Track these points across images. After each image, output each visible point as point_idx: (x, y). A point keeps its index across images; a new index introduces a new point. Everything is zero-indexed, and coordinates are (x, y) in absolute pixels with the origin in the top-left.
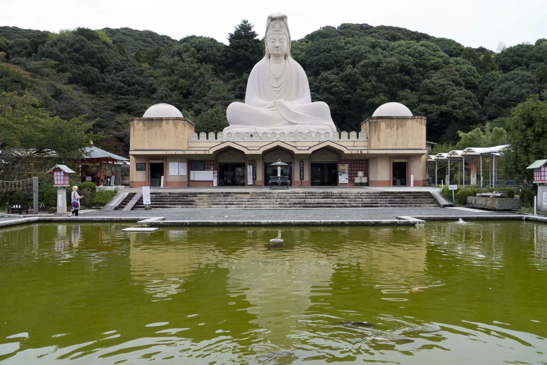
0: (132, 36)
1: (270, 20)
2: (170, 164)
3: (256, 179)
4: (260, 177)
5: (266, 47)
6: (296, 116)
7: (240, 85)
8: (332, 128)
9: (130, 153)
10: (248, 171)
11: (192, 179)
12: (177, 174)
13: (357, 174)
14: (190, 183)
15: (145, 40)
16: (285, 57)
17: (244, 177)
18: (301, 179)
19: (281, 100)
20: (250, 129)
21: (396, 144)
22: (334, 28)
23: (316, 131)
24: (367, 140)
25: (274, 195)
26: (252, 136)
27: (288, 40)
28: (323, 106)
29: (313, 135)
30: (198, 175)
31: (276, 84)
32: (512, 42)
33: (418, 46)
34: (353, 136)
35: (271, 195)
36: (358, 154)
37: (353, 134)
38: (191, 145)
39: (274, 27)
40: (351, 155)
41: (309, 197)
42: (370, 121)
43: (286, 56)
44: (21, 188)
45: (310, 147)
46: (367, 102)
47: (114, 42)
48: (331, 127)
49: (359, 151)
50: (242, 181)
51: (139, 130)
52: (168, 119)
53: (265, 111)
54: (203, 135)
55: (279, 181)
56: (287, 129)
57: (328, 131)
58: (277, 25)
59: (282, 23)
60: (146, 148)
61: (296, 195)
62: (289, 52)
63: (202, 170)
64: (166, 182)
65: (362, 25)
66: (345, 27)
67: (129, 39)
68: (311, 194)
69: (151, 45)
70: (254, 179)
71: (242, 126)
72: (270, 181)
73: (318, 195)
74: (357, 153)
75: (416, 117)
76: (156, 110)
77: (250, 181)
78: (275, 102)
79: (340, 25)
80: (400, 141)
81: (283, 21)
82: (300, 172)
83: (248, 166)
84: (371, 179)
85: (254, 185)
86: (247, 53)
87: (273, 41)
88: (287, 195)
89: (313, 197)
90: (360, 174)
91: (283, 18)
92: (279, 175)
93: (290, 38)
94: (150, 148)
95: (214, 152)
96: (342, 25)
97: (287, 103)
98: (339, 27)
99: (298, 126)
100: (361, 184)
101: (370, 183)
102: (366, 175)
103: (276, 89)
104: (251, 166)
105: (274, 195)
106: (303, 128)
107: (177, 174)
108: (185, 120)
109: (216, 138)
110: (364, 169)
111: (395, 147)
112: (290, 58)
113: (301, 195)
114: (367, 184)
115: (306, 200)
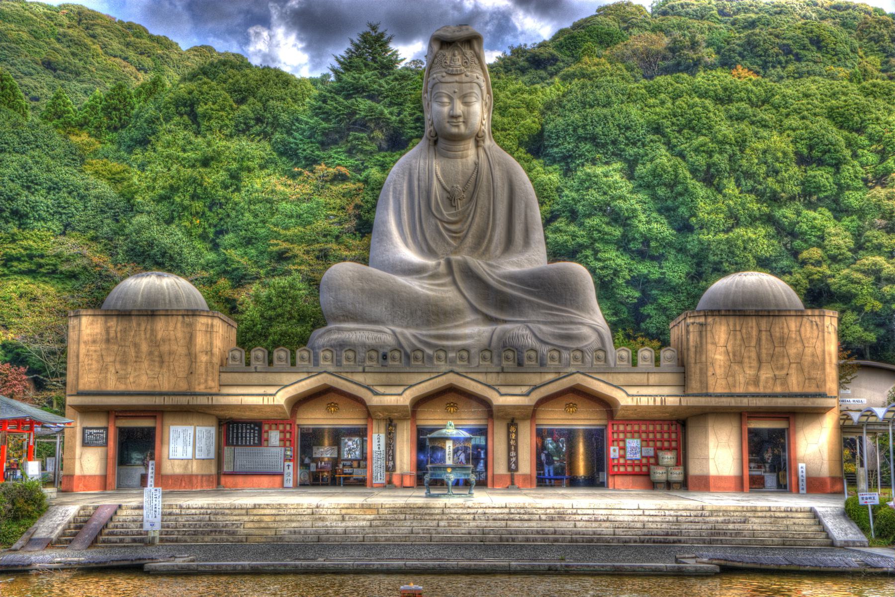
2: (172, 428)
12: (190, 456)
18: (509, 469)
21: (756, 381)
22: (640, 9)
36: (655, 407)
40: (636, 408)
42: (689, 321)
44: (98, 80)
46: (868, 233)
49: (658, 399)
50: (358, 474)
59: (469, 53)
70: (390, 469)
74: (651, 403)
80: (766, 374)
81: (472, 48)
82: (509, 450)
83: (375, 436)
84: (695, 470)
85: (389, 485)
86: (380, 107)
100: (669, 485)
103: (453, 227)
104: (383, 436)
107: (190, 456)
110: (674, 444)
113: (497, 511)
115: (509, 523)
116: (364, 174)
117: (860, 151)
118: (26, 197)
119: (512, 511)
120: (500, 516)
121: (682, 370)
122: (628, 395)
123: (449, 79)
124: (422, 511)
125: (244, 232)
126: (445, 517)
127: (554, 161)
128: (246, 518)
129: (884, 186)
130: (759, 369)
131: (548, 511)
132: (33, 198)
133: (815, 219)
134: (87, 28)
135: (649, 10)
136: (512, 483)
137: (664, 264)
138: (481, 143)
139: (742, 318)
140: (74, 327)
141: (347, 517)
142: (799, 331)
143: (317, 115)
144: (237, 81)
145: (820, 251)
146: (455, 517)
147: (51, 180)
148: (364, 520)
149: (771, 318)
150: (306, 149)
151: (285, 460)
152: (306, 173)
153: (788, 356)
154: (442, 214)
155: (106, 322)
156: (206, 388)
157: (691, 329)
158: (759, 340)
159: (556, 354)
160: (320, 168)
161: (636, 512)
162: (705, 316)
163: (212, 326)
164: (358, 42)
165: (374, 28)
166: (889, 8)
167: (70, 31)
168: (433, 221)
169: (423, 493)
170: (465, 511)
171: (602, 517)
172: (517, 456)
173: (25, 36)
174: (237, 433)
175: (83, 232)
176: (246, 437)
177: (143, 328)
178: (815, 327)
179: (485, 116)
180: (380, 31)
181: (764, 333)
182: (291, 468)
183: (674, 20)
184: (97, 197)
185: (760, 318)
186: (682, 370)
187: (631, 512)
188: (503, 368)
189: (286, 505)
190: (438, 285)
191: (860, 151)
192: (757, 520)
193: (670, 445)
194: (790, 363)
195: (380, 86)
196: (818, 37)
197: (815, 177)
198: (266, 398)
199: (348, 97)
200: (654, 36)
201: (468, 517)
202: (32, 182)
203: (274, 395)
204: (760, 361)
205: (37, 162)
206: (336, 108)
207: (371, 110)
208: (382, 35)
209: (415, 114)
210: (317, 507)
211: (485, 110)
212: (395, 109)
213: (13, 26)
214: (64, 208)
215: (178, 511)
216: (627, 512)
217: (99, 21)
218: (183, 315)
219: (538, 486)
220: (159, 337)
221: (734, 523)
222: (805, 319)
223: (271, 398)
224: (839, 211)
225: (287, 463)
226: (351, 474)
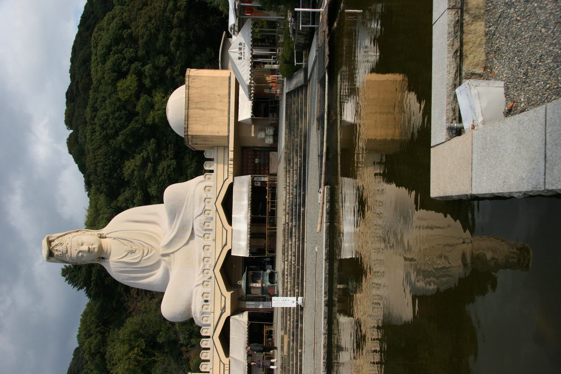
1: (52, 259)
21: (222, 111)
23: (201, 282)
32: (81, 173)
36: (234, 164)
49: (230, 162)
57: (205, 196)
62: (96, 232)
66: (69, 122)
74: (232, 166)
80: (218, 106)
81: (53, 241)
95: (228, 289)
104: (248, 303)
111: (227, 113)
112: (104, 231)
121: (216, 148)
122: (228, 178)
123: (69, 252)
130: (216, 109)
135: (71, 131)
138: (104, 235)
154: (139, 257)
158: (201, 109)
159: (207, 212)
166: (86, 2)
168: (142, 262)
186: (216, 148)
190: (174, 261)
198: (226, 369)
203: (224, 364)
204: (212, 109)
219: (277, 151)
222: (190, 85)
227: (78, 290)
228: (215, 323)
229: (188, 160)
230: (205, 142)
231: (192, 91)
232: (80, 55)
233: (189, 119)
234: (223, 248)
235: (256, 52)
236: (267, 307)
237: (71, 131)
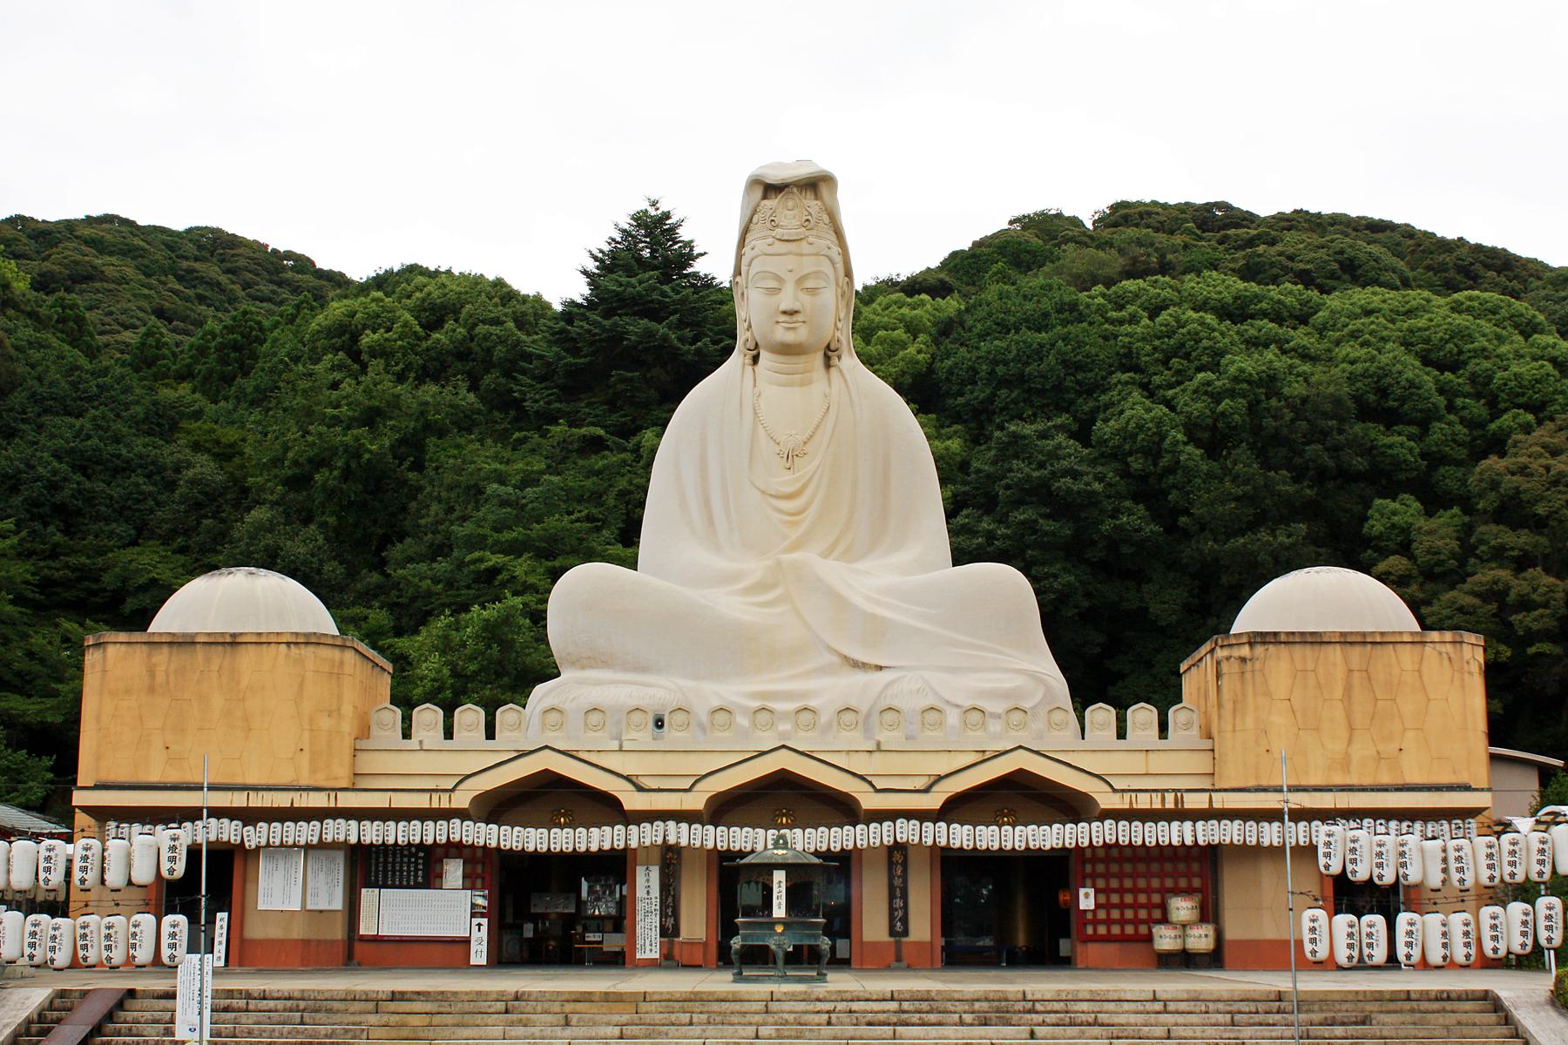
0: (128, 252)
1: (759, 192)
3: (676, 931)
4: (696, 923)
5: (741, 314)
6: (877, 629)
7: (622, 483)
8: (1049, 692)
9: (79, 798)
10: (640, 893)
11: (366, 928)
13: (1164, 907)
14: (355, 949)
15: (190, 271)
16: (827, 358)
17: (620, 921)
18: (892, 932)
19: (809, 557)
20: (658, 691)
21: (1345, 763)
22: (1075, 222)
23: (968, 704)
24: (1207, 744)
25: (746, 1007)
26: (659, 723)
27: (843, 280)
28: (1005, 586)
29: (953, 717)
30: (394, 912)
31: (784, 481)
33: (1438, 312)
34: (1102, 726)
35: (737, 1006)
37: (1142, 715)
38: (369, 763)
39: (774, 224)
41: (915, 1018)
42: (1220, 653)
43: (829, 355)
45: (940, 778)
47: (43, 284)
48: (1041, 682)
49: (1170, 798)
50: (612, 942)
51: (128, 691)
52: (261, 641)
53: (731, 605)
54: (428, 716)
55: (780, 941)
56: (832, 690)
58: (788, 212)
60: (154, 777)
61: (856, 1006)
63: (417, 886)
64: (243, 941)
65: (1209, 207)
66: (1123, 215)
67: (110, 265)
68: (925, 1006)
69: (222, 294)
70: (669, 931)
71: (619, 676)
72: (736, 943)
73: (960, 1007)
75: (1434, 635)
76: (206, 601)
77: (648, 943)
78: (779, 564)
79: (1103, 204)
80: (1362, 750)
81: (817, 196)
82: (892, 897)
83: (640, 871)
85: (670, 960)
86: (662, 329)
87: (772, 284)
88: (811, 1007)
89: (932, 1017)
90: (1182, 908)
91: (816, 185)
92: (779, 911)
93: (848, 274)
94: (173, 777)
96: (1116, 207)
97: (833, 571)
98: (1103, 221)
99: (885, 676)
100: (1184, 960)
101: (1227, 953)
102: (1209, 913)
105: (746, 1007)
106: (908, 686)
108: (343, 647)
109: (490, 734)
110: (1196, 882)
111: (1338, 779)
112: (850, 363)
114: (1215, 959)
116: (634, 440)
117: (1459, 401)
118: (78, 483)
119: (906, 1005)
120: (881, 1017)
124: (725, 1006)
125: (430, 536)
126: (770, 1019)
127: (957, 418)
128: (373, 1019)
129: (1502, 455)
130: (1349, 744)
131: (977, 1006)
132: (88, 485)
133: (1394, 513)
134: (222, 261)
135: (1089, 225)
136: (899, 959)
137: (1145, 588)
138: (835, 361)
139: (1316, 647)
140: (93, 666)
141: (574, 1019)
142: (1419, 671)
143: (556, 342)
144: (429, 294)
145: (1404, 561)
146: (791, 1017)
147: (119, 456)
148: (608, 1024)
149: (1369, 647)
150: (535, 399)
151: (473, 915)
152: (536, 437)
153: (1401, 716)
155: (150, 655)
156: (328, 779)
157: (1225, 667)
158: (1348, 689)
160: (559, 430)
161: (1149, 1006)
162: (1251, 644)
163: (342, 663)
164: (627, 227)
165: (654, 204)
167: (197, 265)
169: (728, 976)
170: (811, 1007)
171: (1084, 1017)
172: (905, 907)
173: (130, 272)
174: (386, 862)
175: (166, 540)
176: (401, 871)
177: (215, 667)
178: (1446, 663)
179: (842, 315)
180: (664, 208)
181: (1356, 674)
182: (485, 928)
183: (1131, 232)
184: (193, 482)
185: (1348, 647)
187: (1140, 1007)
188: (879, 744)
189: (456, 993)
190: (761, 605)
191: (1459, 401)
192: (1387, 1018)
193: (1190, 883)
194: (1405, 730)
195: (663, 294)
196: (1351, 260)
197: (1391, 446)
198: (435, 796)
199: (607, 314)
200: (1101, 254)
201: (817, 1018)
202: (89, 459)
204: (1351, 728)
205: (99, 427)
206: (589, 331)
207: (649, 334)
208: (667, 216)
209: (721, 341)
210: (517, 998)
211: (842, 306)
212: (687, 333)
213: (113, 259)
214: (139, 501)
215: (242, 1003)
216: (1132, 1006)
217: (240, 251)
218: (288, 644)
220: (244, 682)
221: (1343, 1024)
222: (1428, 648)
223: (445, 797)
224: (1433, 502)
225: (476, 921)
226: (601, 942)
227: (585, 273)
228: (581, 755)
229: (1121, 642)
230: (1228, 706)
231: (1407, 655)
232: (1375, 249)
233: (1308, 647)
234: (627, 778)
235: (648, 943)
236: (639, 942)
237: (1089, 225)
